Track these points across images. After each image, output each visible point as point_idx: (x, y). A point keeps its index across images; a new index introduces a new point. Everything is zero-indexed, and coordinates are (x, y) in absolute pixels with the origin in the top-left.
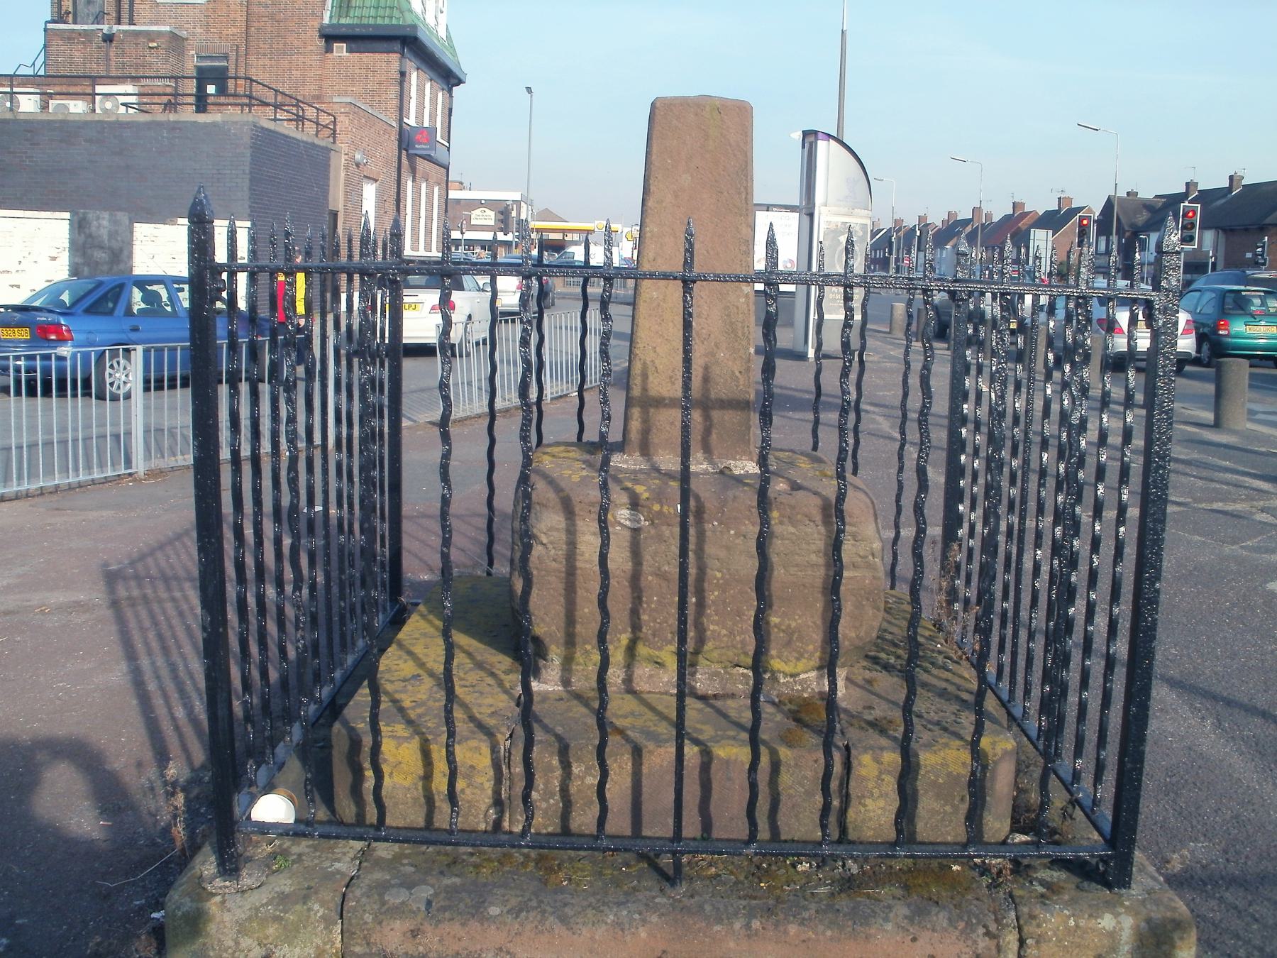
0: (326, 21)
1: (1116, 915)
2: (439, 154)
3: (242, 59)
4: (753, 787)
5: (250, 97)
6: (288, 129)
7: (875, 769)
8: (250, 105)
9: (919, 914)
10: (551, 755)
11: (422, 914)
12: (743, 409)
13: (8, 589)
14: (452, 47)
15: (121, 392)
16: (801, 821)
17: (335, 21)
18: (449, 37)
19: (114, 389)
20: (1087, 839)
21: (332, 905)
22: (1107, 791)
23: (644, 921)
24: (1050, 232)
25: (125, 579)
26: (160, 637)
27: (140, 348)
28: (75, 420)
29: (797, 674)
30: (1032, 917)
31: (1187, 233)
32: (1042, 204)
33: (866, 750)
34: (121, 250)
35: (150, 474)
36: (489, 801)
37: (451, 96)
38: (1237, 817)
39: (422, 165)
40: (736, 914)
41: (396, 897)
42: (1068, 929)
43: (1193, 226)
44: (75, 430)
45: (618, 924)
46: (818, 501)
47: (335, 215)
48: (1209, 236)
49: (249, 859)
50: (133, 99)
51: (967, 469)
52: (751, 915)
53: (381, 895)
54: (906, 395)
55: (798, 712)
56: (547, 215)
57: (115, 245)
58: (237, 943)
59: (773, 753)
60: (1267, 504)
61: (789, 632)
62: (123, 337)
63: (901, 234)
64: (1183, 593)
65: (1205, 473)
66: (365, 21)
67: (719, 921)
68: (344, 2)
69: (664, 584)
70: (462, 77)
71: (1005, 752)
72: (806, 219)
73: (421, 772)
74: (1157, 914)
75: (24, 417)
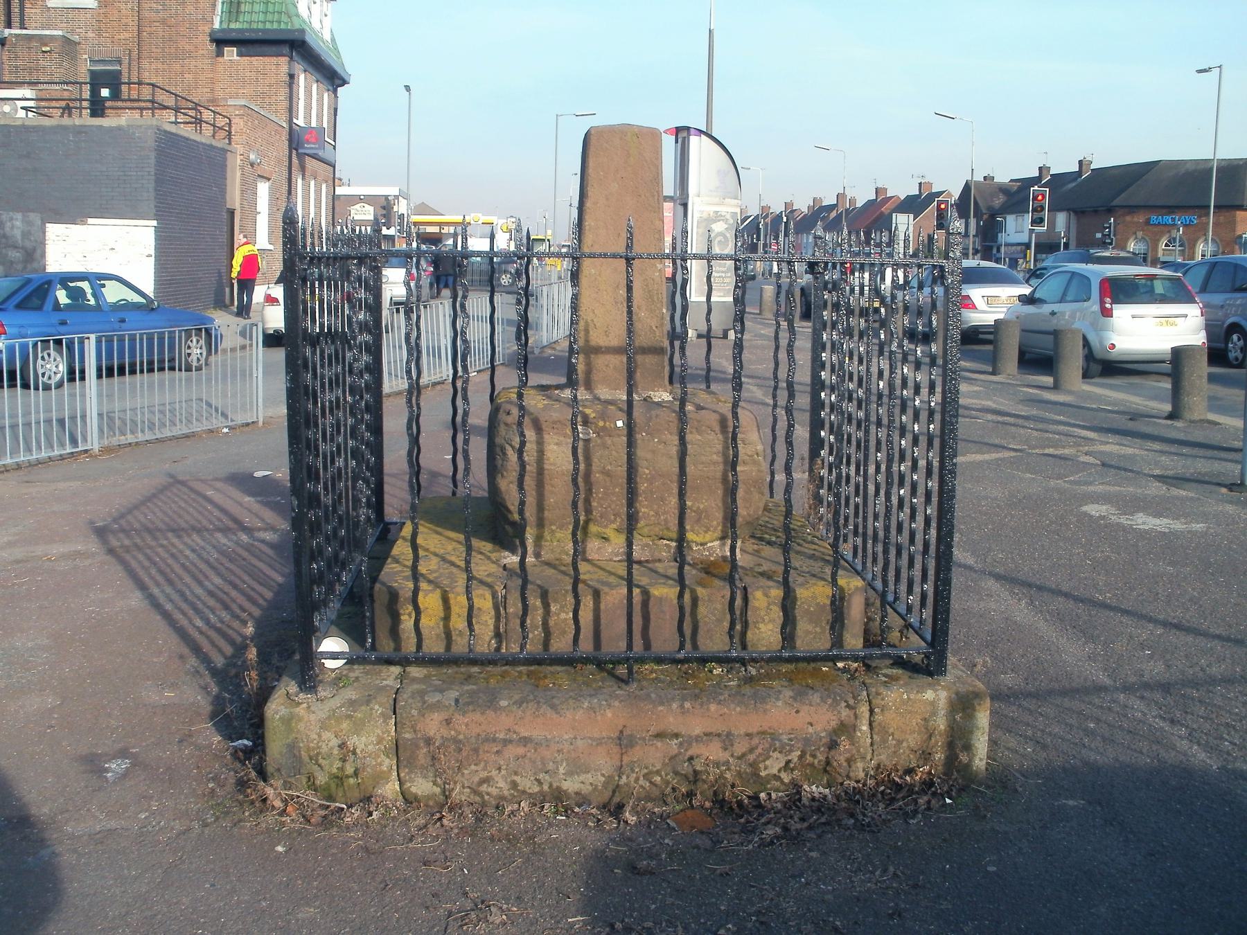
0: (217, 26)
1: (936, 691)
2: (326, 153)
3: (135, 63)
4: (681, 608)
5: (153, 102)
6: (187, 131)
7: (765, 604)
8: (153, 109)
9: (799, 696)
10: (535, 598)
11: (453, 708)
12: (659, 354)
13: (10, 544)
14: (336, 49)
15: (53, 382)
16: (714, 640)
17: (225, 26)
18: (333, 40)
19: (45, 379)
20: (914, 647)
21: (388, 706)
22: (927, 614)
23: (609, 706)
24: (911, 216)
25: (113, 532)
26: (162, 572)
27: (93, 337)
28: (37, 405)
29: (708, 543)
30: (878, 694)
31: (1037, 215)
32: (903, 189)
33: (758, 588)
34: (34, 250)
35: (106, 450)
36: (491, 634)
37: (336, 97)
38: (1037, 659)
39: (311, 164)
40: (673, 699)
41: (433, 698)
42: (902, 699)
43: (1043, 209)
44: (37, 412)
45: (592, 708)
46: (717, 417)
47: (232, 213)
48: (1061, 218)
49: (321, 681)
50: (31, 104)
51: (829, 425)
52: (684, 699)
53: (422, 697)
54: (776, 369)
55: (708, 569)
56: (423, 209)
57: (28, 244)
58: (320, 736)
59: (693, 592)
60: (1091, 449)
61: (699, 512)
62: (53, 330)
63: (768, 220)
64: (1012, 516)
65: (1040, 426)
66: (254, 26)
67: (662, 704)
68: (234, 8)
69: (608, 479)
70: (346, 78)
71: (857, 588)
72: (680, 209)
73: (442, 615)
74: (963, 689)
75: (9, 400)
